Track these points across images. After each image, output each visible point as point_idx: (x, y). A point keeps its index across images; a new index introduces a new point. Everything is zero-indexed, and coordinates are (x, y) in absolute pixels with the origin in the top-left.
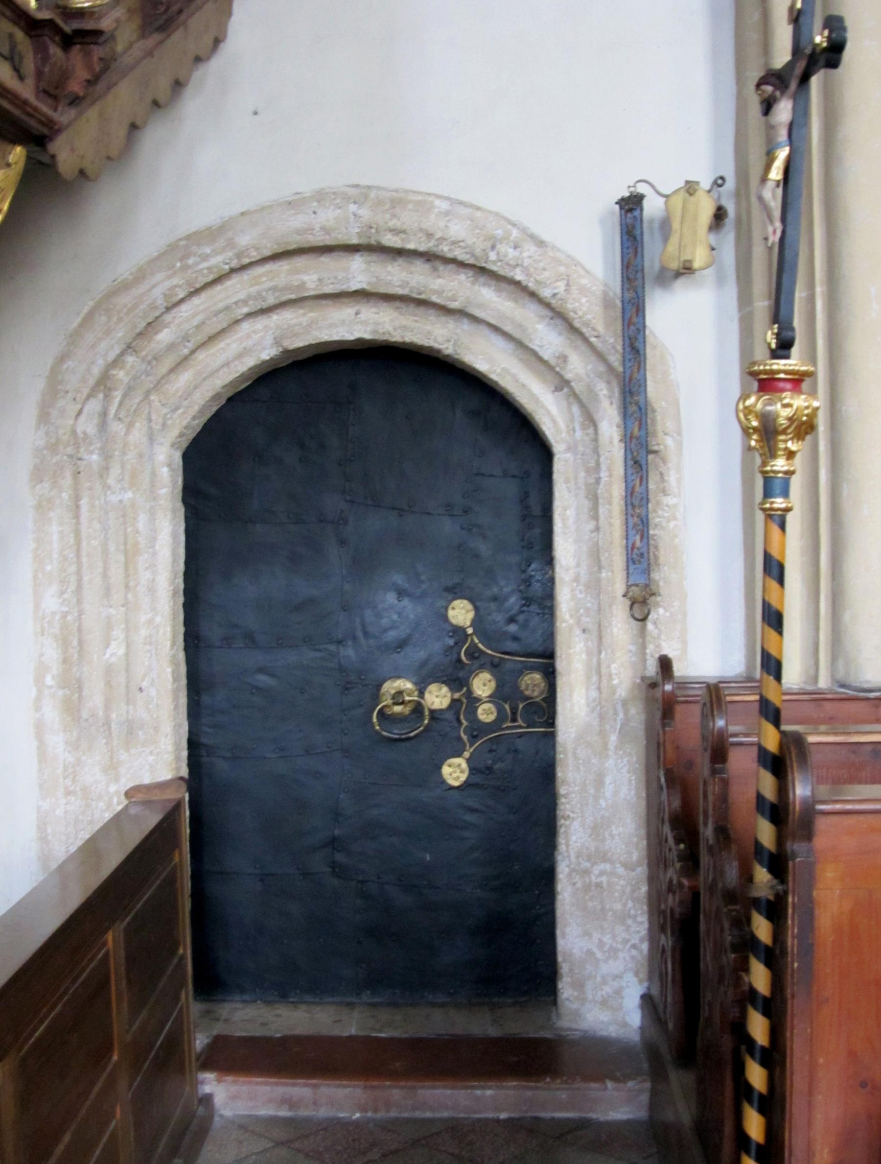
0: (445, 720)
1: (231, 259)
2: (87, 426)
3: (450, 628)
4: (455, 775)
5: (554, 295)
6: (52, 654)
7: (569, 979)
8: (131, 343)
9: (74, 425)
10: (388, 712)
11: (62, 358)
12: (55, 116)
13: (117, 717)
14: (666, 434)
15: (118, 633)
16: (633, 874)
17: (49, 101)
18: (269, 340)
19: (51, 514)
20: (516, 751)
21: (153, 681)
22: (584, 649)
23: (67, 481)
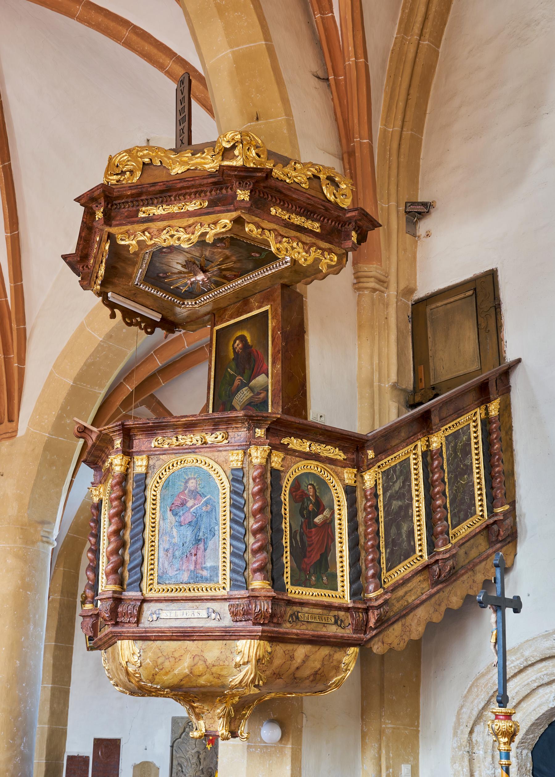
1: (523, 662)
11: (462, 707)
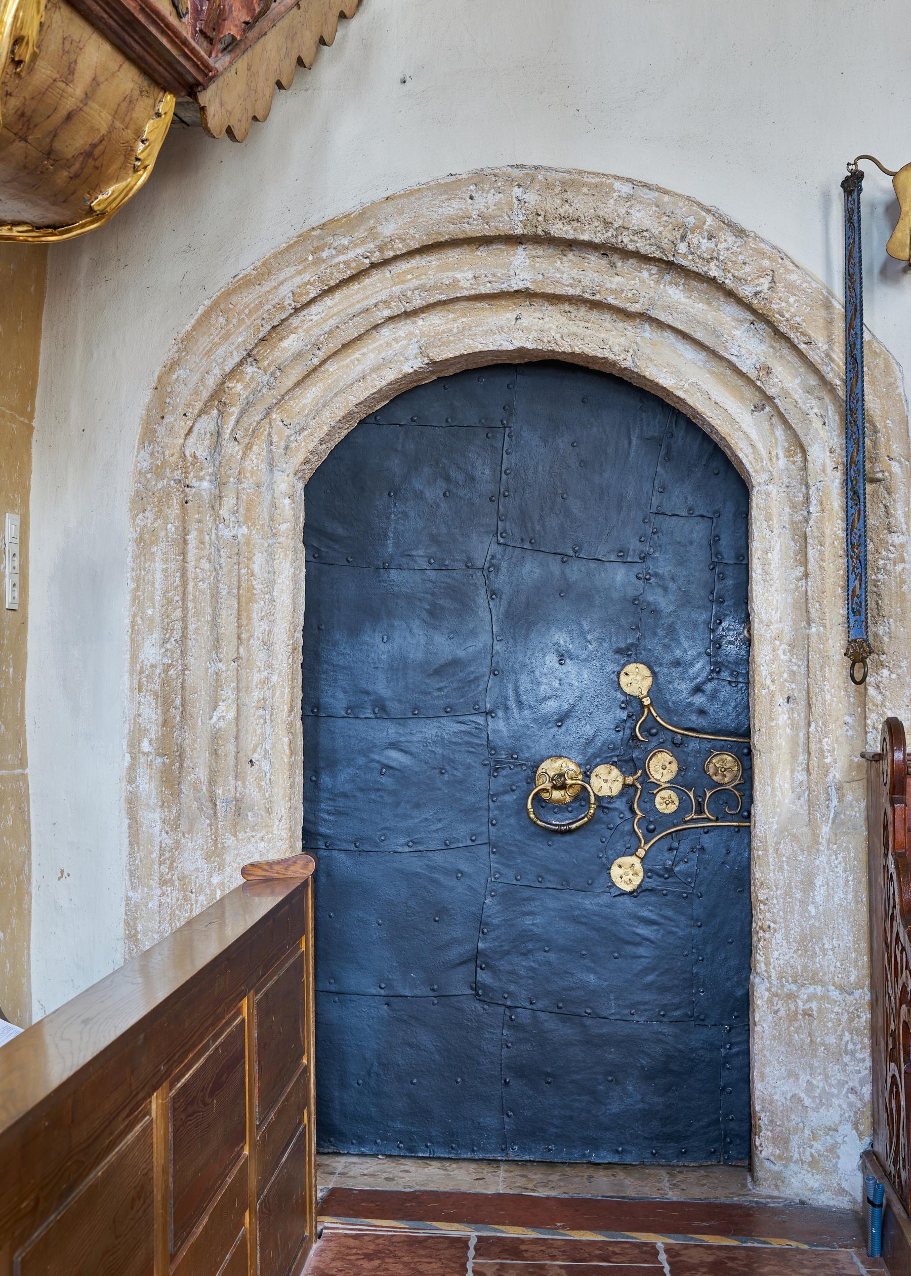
0: (615, 809)
2: (198, 447)
3: (623, 698)
4: (626, 878)
5: (756, 294)
6: (151, 714)
7: (769, 1133)
8: (251, 351)
9: (184, 445)
10: (545, 796)
11: (172, 366)
12: (211, 61)
13: (223, 792)
14: (891, 459)
15: (228, 692)
16: (851, 998)
17: (205, 44)
18: (413, 350)
19: (154, 549)
20: (703, 849)
21: (266, 751)
22: (789, 722)
23: (175, 510)
